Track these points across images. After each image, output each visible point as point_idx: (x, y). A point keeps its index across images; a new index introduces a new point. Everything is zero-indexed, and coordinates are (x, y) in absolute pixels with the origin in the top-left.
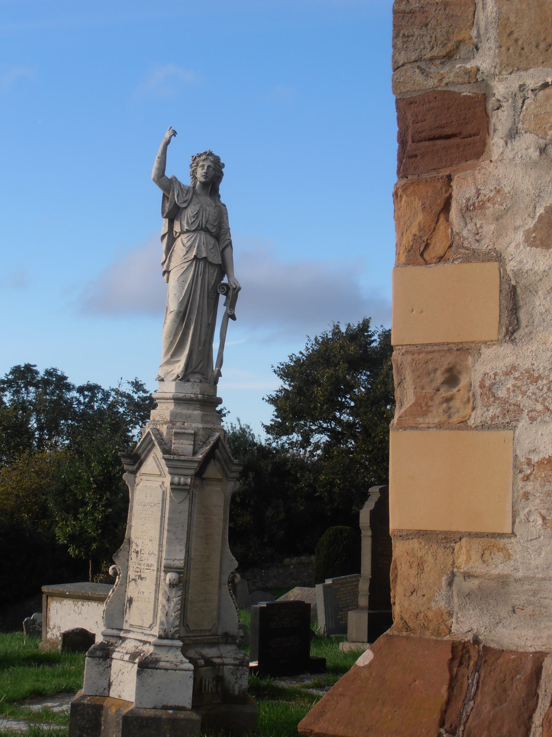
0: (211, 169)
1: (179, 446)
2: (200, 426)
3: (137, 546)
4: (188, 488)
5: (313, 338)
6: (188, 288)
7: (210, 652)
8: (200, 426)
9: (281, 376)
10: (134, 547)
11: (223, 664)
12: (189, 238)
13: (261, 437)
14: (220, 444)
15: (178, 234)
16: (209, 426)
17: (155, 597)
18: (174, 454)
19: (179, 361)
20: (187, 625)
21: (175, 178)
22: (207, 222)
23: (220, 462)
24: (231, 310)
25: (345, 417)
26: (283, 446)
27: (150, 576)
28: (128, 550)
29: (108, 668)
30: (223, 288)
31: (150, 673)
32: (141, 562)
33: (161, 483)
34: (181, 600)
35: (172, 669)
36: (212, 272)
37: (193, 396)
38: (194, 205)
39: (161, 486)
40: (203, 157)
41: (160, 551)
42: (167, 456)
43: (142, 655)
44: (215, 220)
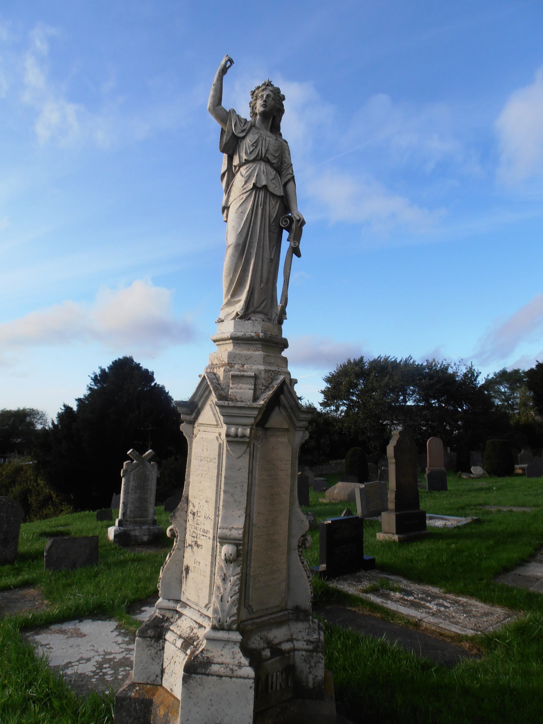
0: (270, 99)
1: (237, 390)
2: (262, 367)
3: (194, 506)
4: (247, 440)
5: (339, 365)
6: (247, 219)
7: (278, 634)
8: (262, 367)
9: (326, 382)
10: (191, 507)
11: (294, 650)
13: (319, 408)
14: (285, 388)
15: (237, 168)
16: (273, 368)
17: (211, 571)
18: (232, 400)
19: (240, 300)
20: (250, 606)
22: (267, 151)
23: (285, 408)
24: (295, 243)
25: (354, 398)
26: (327, 411)
27: (207, 543)
28: (185, 509)
29: (160, 650)
30: (286, 221)
31: (199, 680)
32: (197, 526)
33: (217, 435)
34: (241, 579)
35: (227, 676)
36: (274, 204)
37: (253, 334)
38: (253, 134)
39: (217, 438)
41: (217, 515)
42: (221, 403)
43: (195, 643)
44: (276, 151)
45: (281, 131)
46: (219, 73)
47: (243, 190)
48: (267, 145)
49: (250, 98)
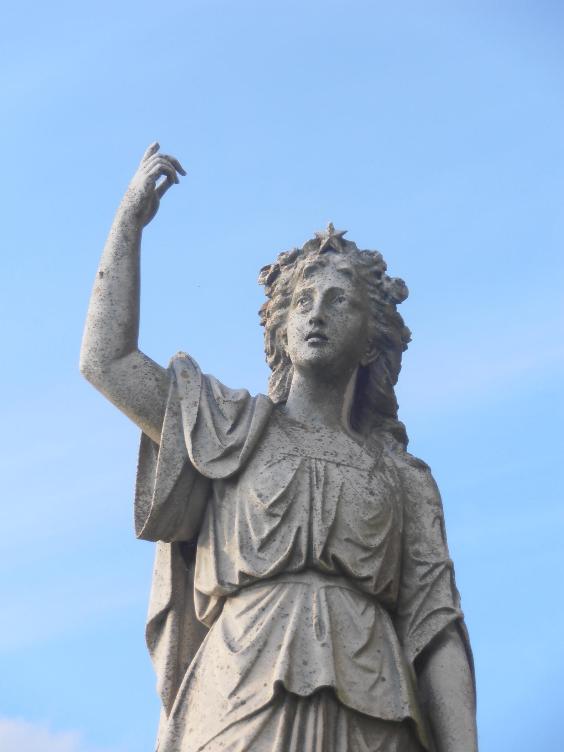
15: (213, 603)
21: (189, 363)
22: (332, 533)
40: (304, 263)
44: (374, 525)
46: (123, 224)
47: (236, 707)
48: (332, 505)
49: (259, 295)
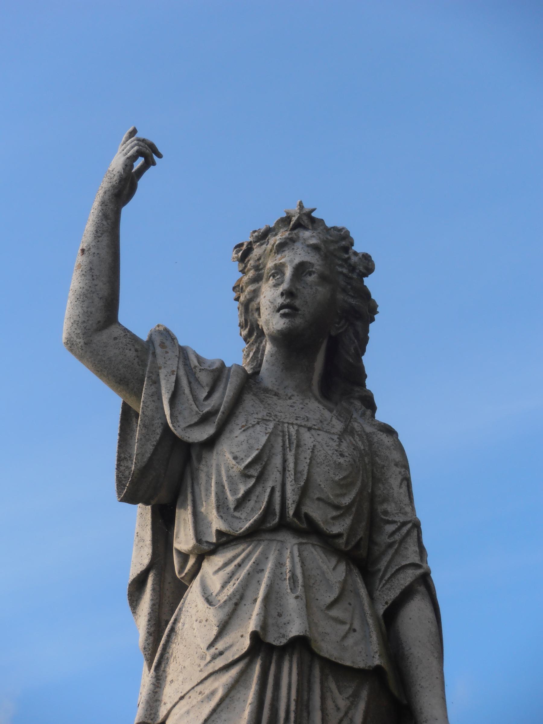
12: (231, 567)
21: (166, 336)
22: (304, 492)
36: (343, 703)
44: (344, 485)
45: (370, 384)
47: (214, 658)
48: (304, 467)
49: (232, 272)
